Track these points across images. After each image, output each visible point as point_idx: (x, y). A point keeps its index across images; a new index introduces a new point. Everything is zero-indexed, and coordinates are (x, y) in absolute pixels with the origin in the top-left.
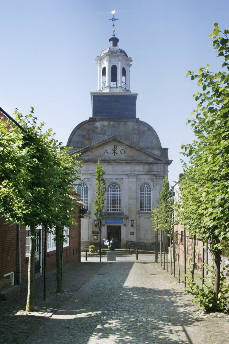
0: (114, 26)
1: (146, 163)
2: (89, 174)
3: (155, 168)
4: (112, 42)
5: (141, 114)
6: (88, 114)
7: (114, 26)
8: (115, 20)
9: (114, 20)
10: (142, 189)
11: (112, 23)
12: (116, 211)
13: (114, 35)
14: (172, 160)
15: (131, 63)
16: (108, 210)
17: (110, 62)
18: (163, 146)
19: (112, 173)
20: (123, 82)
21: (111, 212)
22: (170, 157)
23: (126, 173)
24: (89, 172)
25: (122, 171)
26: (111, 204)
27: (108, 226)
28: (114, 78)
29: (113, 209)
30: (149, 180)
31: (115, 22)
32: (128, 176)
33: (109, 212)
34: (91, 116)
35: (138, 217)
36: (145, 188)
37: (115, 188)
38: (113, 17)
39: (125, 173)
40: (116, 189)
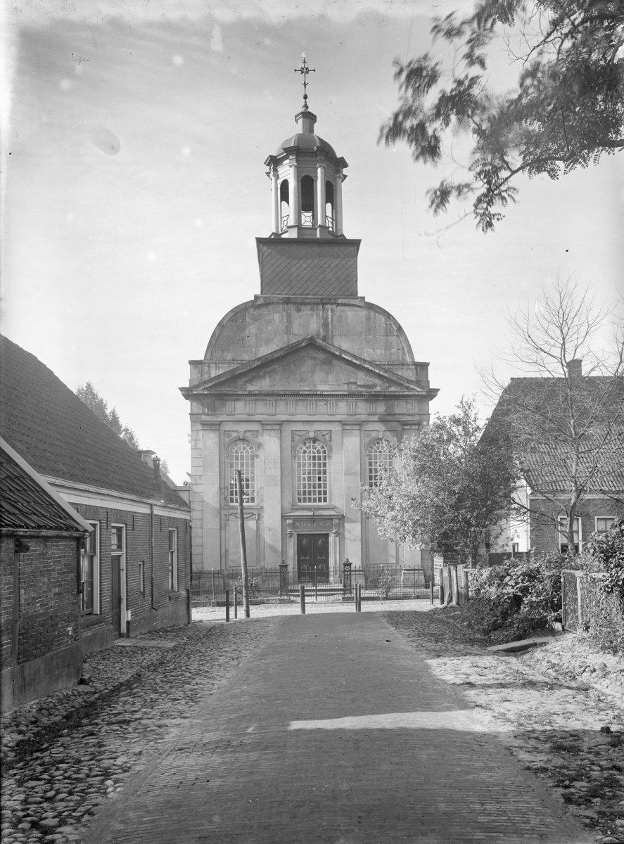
0: (305, 85)
1: (339, 395)
2: (337, 421)
3: (401, 408)
4: (300, 121)
5: (369, 286)
6: (247, 286)
7: (305, 85)
8: (307, 72)
9: (305, 71)
10: (373, 454)
11: (301, 77)
12: (233, 502)
13: (306, 106)
14: (437, 388)
15: (345, 171)
16: (300, 501)
17: (299, 169)
18: (418, 359)
19: (246, 417)
20: (327, 216)
21: (305, 504)
22: (434, 382)
23: (338, 418)
24: (337, 416)
25: (228, 415)
26: (314, 487)
27: (300, 535)
28: (307, 203)
29: (310, 499)
30: (388, 433)
31: (307, 75)
32: (262, 424)
33: (300, 504)
34: (258, 292)
35: (226, 515)
36: (242, 452)
37: (314, 453)
38: (303, 65)
39: (233, 420)
40: (317, 455)
